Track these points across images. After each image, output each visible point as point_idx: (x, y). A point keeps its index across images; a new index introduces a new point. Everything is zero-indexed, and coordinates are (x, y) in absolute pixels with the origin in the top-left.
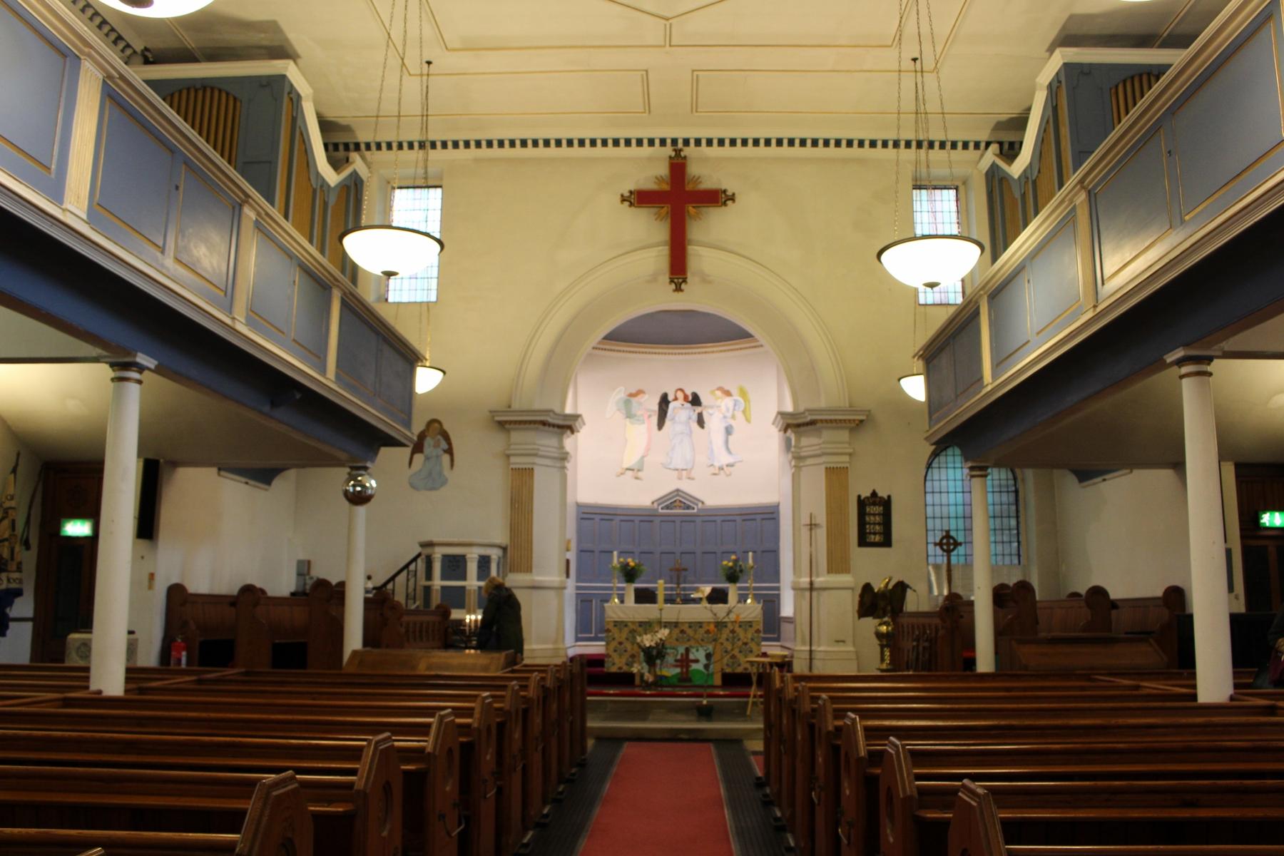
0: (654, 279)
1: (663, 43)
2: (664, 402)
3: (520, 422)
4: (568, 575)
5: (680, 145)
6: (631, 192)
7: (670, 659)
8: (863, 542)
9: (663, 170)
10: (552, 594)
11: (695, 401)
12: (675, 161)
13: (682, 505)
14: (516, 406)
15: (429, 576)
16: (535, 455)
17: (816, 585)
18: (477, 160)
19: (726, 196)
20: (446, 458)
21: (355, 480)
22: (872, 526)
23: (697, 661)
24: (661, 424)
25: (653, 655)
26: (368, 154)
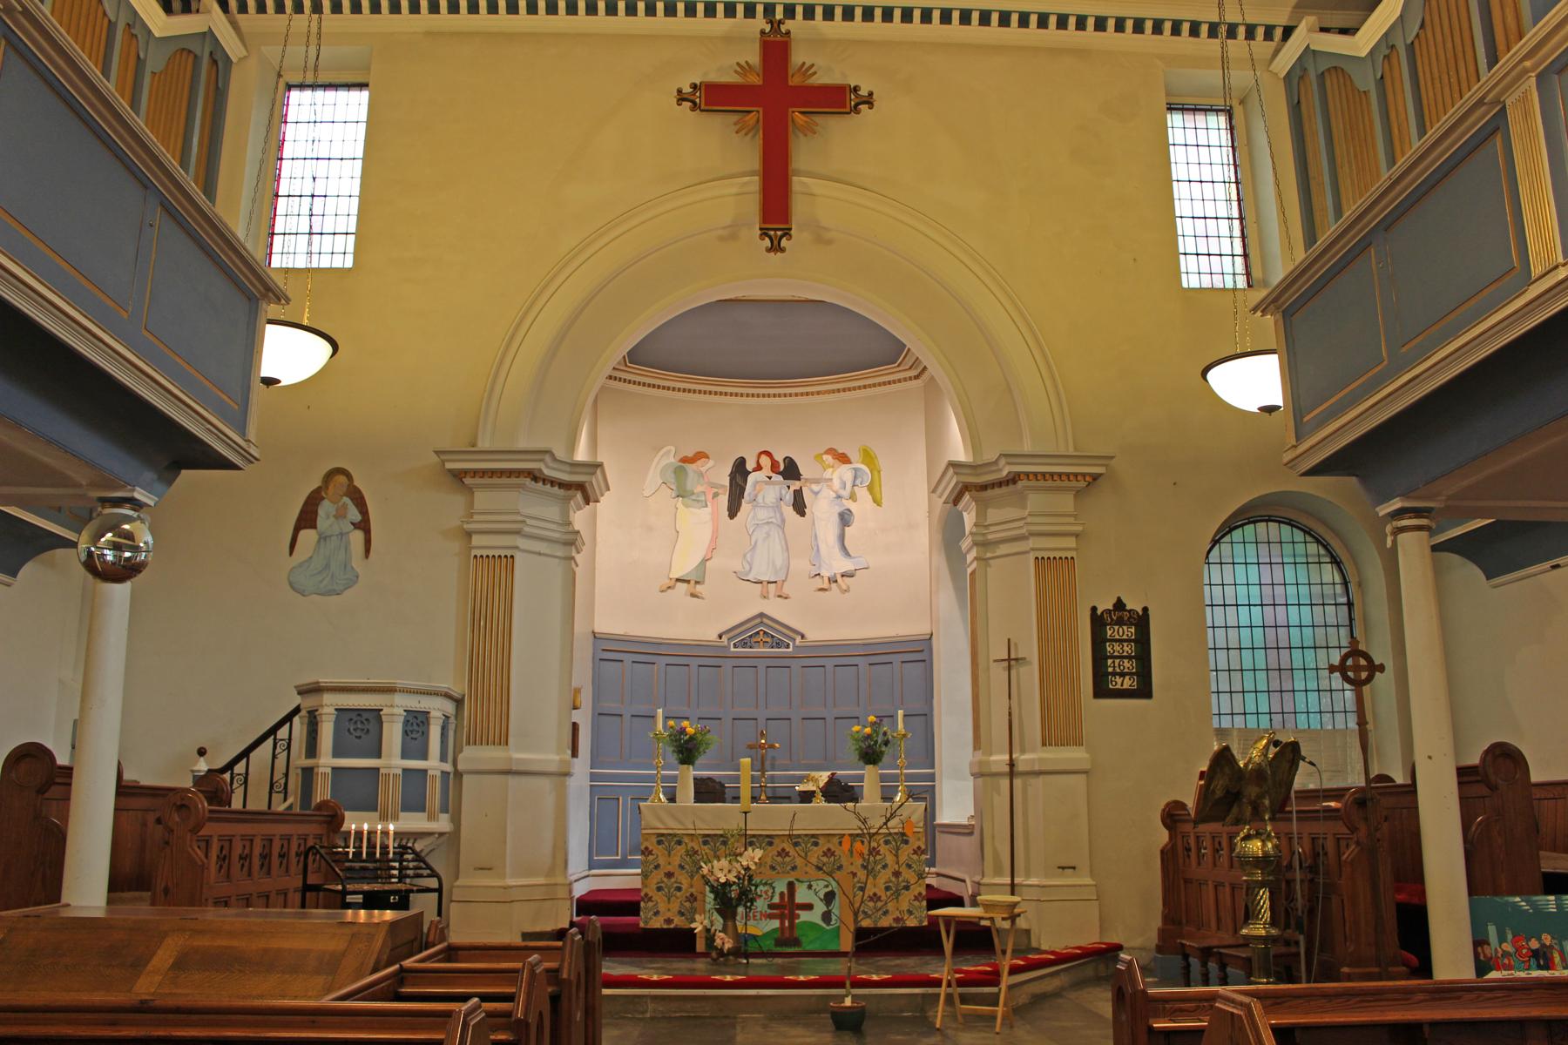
0: (731, 234)
2: (740, 471)
4: (575, 754)
5: (779, 15)
7: (761, 905)
8: (1102, 690)
10: (545, 784)
11: (790, 471)
12: (772, 38)
13: (769, 640)
14: (484, 443)
15: (312, 749)
16: (518, 532)
17: (1020, 767)
20: (357, 537)
21: (115, 528)
23: (809, 907)
24: (733, 511)
25: (730, 901)
26: (240, 17)
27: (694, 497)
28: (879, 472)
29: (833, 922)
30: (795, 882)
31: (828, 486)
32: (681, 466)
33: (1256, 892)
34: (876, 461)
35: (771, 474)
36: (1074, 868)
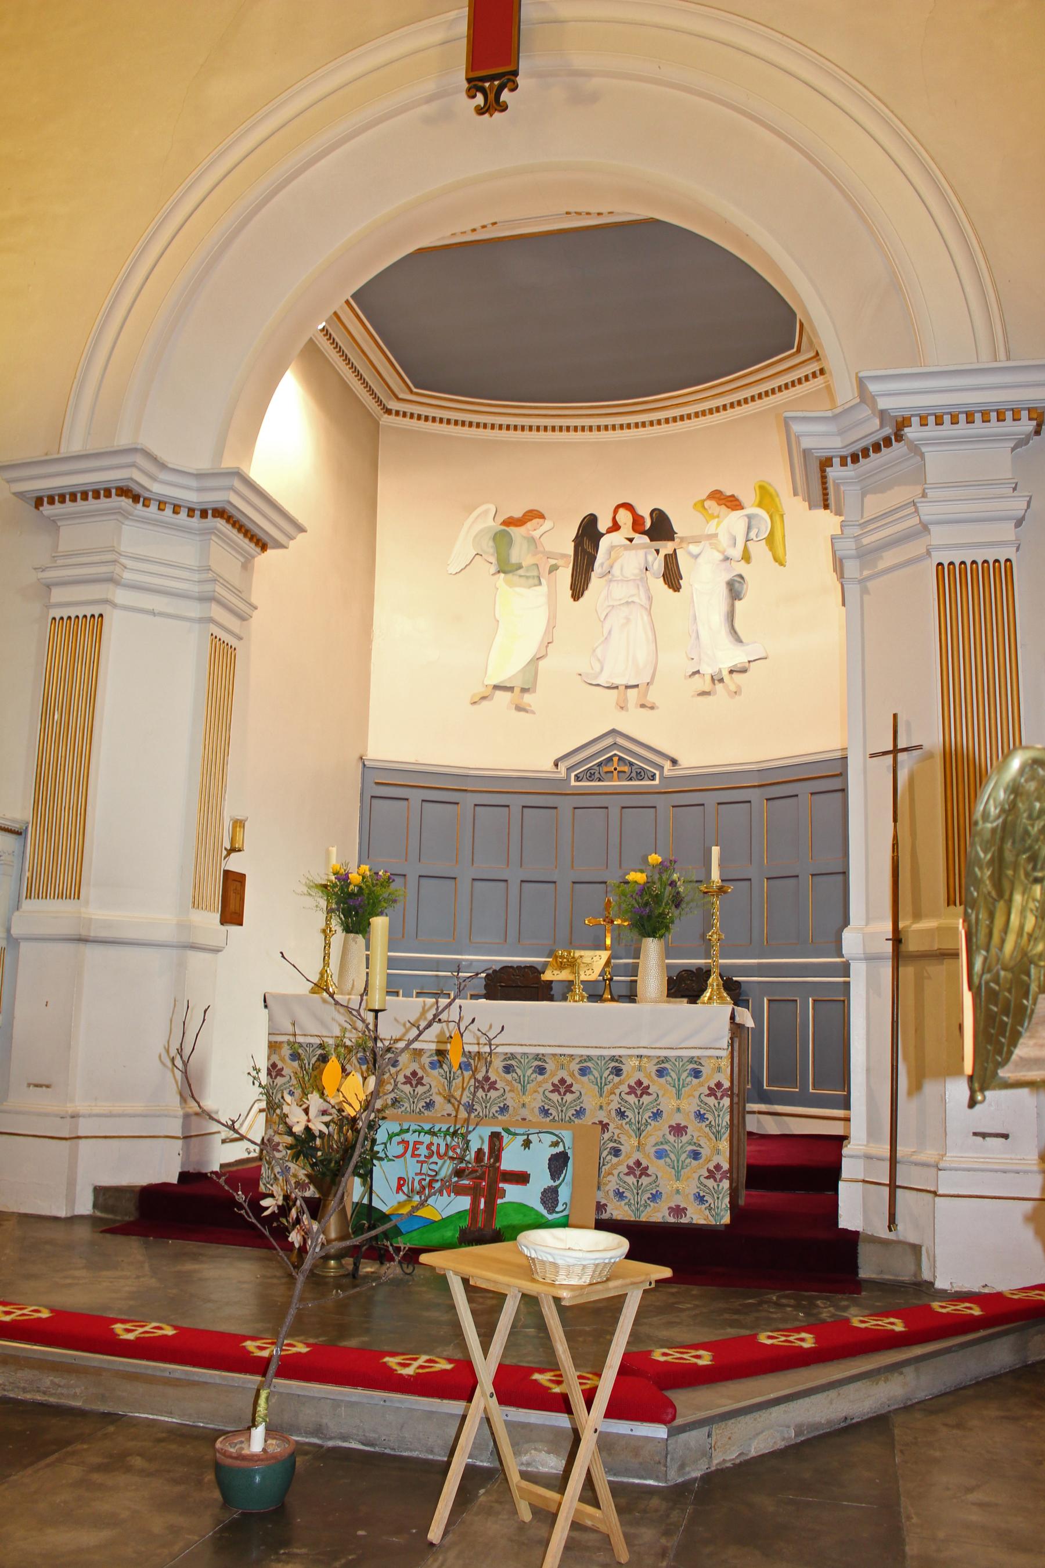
13: (626, 769)
17: (912, 945)
23: (522, 1178)
24: (578, 589)
27: (521, 572)
28: (782, 516)
29: (560, 1208)
30: (504, 1134)
31: (711, 544)
32: (504, 530)
34: (777, 500)
35: (632, 535)
36: (1006, 1136)
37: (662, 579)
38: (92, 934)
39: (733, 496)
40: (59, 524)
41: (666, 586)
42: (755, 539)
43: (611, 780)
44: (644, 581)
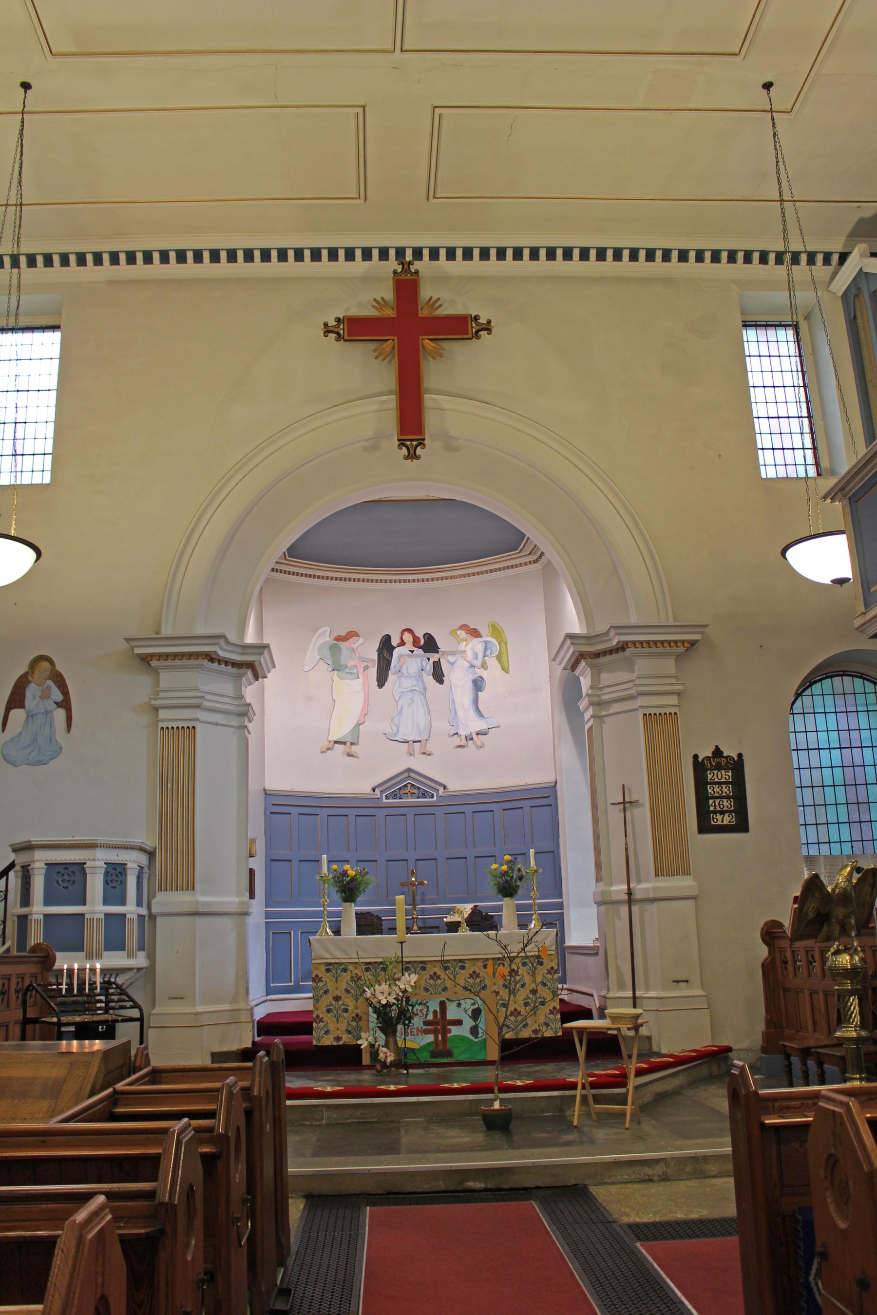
0: (374, 445)
1: (390, 47)
2: (386, 647)
3: (175, 656)
4: (252, 895)
5: (409, 257)
6: (338, 320)
7: (417, 1022)
8: (705, 827)
9: (388, 293)
11: (430, 645)
12: (403, 277)
13: (415, 791)
15: (26, 900)
16: (198, 706)
17: (637, 895)
18: (112, 283)
19: (478, 324)
20: (61, 714)
22: (717, 801)
23: (459, 1023)
24: (381, 681)
27: (347, 670)
28: (506, 644)
29: (480, 1035)
30: (446, 1001)
32: (336, 644)
33: (846, 1000)
36: (687, 981)
37: (432, 676)
38: (201, 910)
39: (475, 629)
40: (159, 671)
41: (437, 683)
42: (489, 656)
43: (407, 798)
44: (421, 677)
